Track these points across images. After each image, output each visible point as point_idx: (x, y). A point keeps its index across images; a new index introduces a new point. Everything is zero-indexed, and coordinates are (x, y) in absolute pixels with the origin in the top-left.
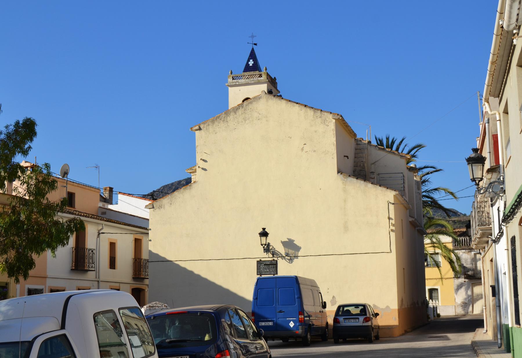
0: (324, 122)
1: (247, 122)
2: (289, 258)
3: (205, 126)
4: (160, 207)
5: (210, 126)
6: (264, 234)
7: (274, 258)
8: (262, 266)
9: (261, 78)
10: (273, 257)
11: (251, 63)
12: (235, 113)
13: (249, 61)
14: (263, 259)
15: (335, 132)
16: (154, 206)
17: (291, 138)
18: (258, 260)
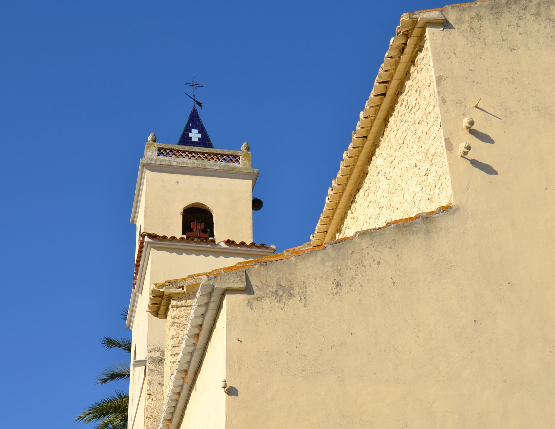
3: (466, 16)
4: (284, 292)
5: (485, 23)
9: (236, 164)
11: (195, 135)
13: (188, 130)
16: (254, 282)
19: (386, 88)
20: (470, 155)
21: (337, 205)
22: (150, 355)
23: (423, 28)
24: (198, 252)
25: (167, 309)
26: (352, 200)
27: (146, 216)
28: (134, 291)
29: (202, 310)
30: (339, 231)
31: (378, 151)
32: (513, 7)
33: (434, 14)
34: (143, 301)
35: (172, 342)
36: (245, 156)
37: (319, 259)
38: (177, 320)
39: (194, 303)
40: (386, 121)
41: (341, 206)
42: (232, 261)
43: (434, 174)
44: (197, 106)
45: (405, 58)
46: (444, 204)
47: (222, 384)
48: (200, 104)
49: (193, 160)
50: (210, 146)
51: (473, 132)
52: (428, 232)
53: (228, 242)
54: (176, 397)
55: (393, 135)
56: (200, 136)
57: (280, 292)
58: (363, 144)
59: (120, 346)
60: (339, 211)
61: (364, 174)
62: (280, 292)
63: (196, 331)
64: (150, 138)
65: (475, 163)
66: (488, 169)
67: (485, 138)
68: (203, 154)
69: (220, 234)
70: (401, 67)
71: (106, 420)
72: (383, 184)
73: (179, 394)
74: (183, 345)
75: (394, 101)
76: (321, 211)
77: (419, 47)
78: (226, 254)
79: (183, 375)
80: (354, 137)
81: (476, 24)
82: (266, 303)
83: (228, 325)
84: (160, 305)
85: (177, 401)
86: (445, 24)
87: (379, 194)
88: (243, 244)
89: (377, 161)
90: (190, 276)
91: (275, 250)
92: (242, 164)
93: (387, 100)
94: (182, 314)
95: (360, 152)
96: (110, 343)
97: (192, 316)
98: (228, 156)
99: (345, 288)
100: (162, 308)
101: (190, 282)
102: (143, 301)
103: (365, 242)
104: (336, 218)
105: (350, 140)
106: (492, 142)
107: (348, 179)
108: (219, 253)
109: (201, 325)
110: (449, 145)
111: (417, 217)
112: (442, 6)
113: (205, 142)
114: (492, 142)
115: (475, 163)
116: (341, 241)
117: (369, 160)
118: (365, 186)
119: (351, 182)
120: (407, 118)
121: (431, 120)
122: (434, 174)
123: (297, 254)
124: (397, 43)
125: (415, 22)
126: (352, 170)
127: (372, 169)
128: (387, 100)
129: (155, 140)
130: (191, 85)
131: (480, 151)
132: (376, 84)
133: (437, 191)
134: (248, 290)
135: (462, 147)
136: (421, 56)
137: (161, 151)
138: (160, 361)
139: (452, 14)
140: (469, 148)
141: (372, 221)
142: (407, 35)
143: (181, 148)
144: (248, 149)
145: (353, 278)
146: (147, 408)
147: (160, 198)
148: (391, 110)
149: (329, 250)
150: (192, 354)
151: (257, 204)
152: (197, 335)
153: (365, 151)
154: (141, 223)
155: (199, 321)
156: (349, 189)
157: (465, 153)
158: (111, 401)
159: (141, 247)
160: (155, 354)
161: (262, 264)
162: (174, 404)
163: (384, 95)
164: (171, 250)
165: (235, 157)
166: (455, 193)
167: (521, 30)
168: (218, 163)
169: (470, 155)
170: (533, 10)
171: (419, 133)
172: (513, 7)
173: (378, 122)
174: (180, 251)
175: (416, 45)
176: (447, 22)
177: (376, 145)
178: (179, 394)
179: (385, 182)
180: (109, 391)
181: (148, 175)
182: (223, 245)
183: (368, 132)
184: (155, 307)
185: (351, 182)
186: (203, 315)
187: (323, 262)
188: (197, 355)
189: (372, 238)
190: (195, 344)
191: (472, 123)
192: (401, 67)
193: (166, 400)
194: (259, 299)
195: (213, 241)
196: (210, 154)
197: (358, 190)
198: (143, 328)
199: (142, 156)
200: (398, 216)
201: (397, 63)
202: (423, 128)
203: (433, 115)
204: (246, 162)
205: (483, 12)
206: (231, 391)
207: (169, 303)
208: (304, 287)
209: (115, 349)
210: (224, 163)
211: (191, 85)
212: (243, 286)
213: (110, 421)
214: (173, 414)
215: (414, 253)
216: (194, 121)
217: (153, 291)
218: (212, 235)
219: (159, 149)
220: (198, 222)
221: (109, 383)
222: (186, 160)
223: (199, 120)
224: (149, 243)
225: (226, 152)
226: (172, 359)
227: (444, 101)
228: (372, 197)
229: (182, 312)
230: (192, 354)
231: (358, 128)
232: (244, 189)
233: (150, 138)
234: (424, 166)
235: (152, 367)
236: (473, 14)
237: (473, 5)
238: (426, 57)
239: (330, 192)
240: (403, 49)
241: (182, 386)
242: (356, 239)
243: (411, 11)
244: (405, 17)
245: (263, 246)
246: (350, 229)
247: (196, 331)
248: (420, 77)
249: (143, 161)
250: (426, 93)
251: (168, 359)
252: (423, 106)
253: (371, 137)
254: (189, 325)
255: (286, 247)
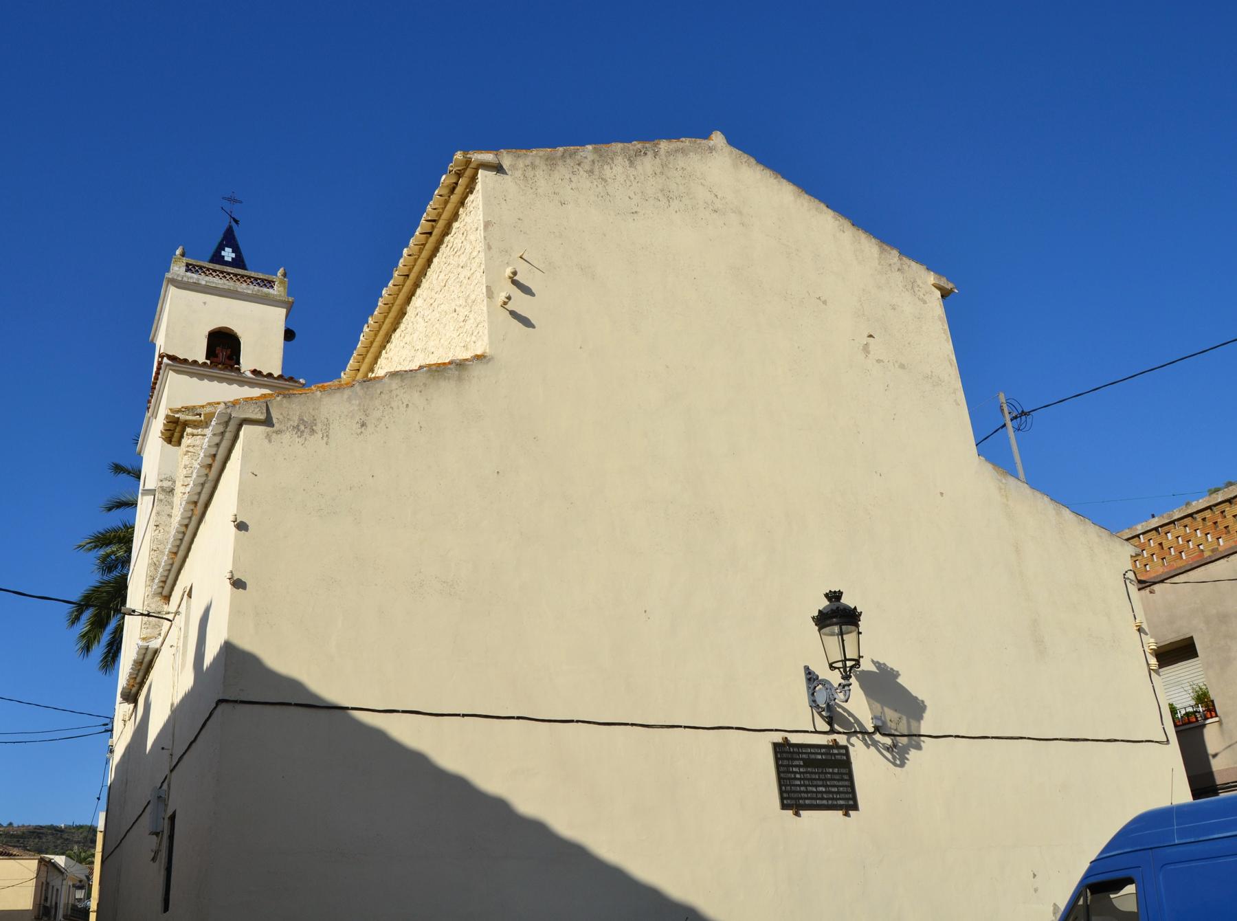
0: (912, 286)
1: (675, 204)
2: (888, 741)
3: (521, 163)
4: (305, 427)
5: (539, 173)
6: (838, 616)
7: (835, 736)
8: (797, 770)
9: (271, 291)
10: (832, 731)
11: (228, 254)
12: (632, 163)
13: (221, 247)
14: (795, 739)
15: (946, 327)
16: (275, 415)
17: (825, 302)
18: (778, 738)
19: (433, 227)
20: (510, 306)
21: (372, 343)
22: (160, 484)
23: (476, 169)
24: (221, 380)
25: (182, 437)
26: (388, 339)
27: (167, 335)
28: (148, 415)
29: (217, 439)
30: (372, 370)
31: (419, 291)
32: (568, 161)
33: (488, 157)
34: (157, 426)
35: (185, 472)
36: (281, 282)
37: (346, 396)
38: (191, 449)
39: (208, 432)
40: (429, 262)
41: (376, 344)
42: (256, 392)
43: (472, 321)
44: (233, 224)
45: (454, 198)
46: (479, 353)
47: (232, 518)
48: (236, 222)
49: (224, 281)
50: (244, 267)
51: (515, 282)
52: (460, 379)
53: (254, 372)
54: (183, 529)
55: (435, 276)
56: (233, 255)
57: (302, 427)
58: (404, 282)
59: (129, 473)
60: (373, 350)
61: (402, 314)
62: (302, 427)
63: (209, 461)
64: (178, 252)
65: (513, 314)
66: (526, 322)
67: (526, 290)
68: (236, 275)
69: (247, 362)
70: (450, 207)
71: (108, 550)
72: (421, 325)
73: (187, 526)
74: (194, 476)
75: (440, 242)
76: (355, 348)
77: (470, 189)
78: (251, 384)
79: (192, 507)
80: (396, 274)
81: (530, 173)
82: (287, 437)
83: (243, 456)
84: (175, 431)
85: (184, 533)
86: (499, 169)
87: (415, 336)
88: (270, 375)
89: (417, 302)
90: (209, 404)
91: (304, 385)
92: (277, 291)
93: (433, 239)
94: (198, 443)
95: (400, 290)
96: (118, 469)
97: (205, 446)
98: (263, 280)
99: (370, 428)
100: (176, 435)
101: (208, 410)
102: (157, 426)
103: (395, 384)
104: (370, 356)
105: (391, 277)
106: (533, 295)
107: (385, 317)
108: (243, 382)
109: (215, 456)
110: (490, 294)
111: (450, 363)
112: (497, 149)
113: (238, 262)
114: (533, 295)
115: (513, 314)
116: (371, 379)
117: (408, 300)
118: (402, 326)
119: (388, 321)
120: (451, 260)
121: (474, 266)
122: (472, 321)
123: (323, 389)
124: (448, 182)
125: (468, 162)
126: (390, 309)
127: (410, 309)
128: (433, 239)
129: (183, 255)
130: (229, 199)
131: (521, 303)
132: (423, 221)
133: (474, 338)
134: (268, 422)
135: (502, 297)
136: (471, 197)
137: (189, 267)
138: (171, 491)
139: (506, 160)
140: (509, 298)
141: (406, 363)
142: (459, 175)
143: (211, 266)
144: (285, 275)
145: (379, 420)
146: (153, 540)
147: (184, 317)
148: (436, 250)
149: (357, 387)
150: (203, 485)
151: (289, 335)
152: (210, 466)
153: (406, 289)
154: (162, 342)
155: (213, 451)
156: (385, 327)
157: (505, 303)
158: (115, 531)
159: (159, 369)
160: (166, 484)
161: (285, 396)
162: (180, 536)
163: (430, 234)
164: (192, 375)
165: (270, 282)
166: (491, 343)
167: (573, 185)
168: (251, 286)
169: (510, 306)
170: (587, 167)
171: (462, 277)
172: (568, 161)
173: (421, 262)
174: (201, 377)
175: (467, 187)
176: (501, 166)
177: (417, 285)
178: (187, 526)
179: (423, 324)
180: (114, 520)
181: (172, 290)
182: (249, 374)
183: (410, 270)
184: (168, 434)
185: (388, 321)
186: (218, 445)
187: (349, 399)
188: (208, 487)
189: (402, 380)
190: (207, 475)
191: (515, 273)
192: (450, 207)
193: (173, 532)
194: (279, 432)
195: (239, 369)
196: (242, 276)
197: (395, 330)
198: (155, 455)
199: (168, 271)
200: (433, 360)
201: (446, 202)
202: (466, 273)
203: (477, 260)
204: (281, 289)
205: (537, 161)
206: (241, 526)
207: (184, 430)
208: (327, 424)
209: (123, 476)
210: (257, 288)
211: (229, 199)
212: (262, 417)
213: (113, 552)
214: (179, 547)
215: (444, 397)
216: (229, 239)
217: (167, 417)
218: (238, 363)
219: (187, 265)
220: (223, 347)
221: (115, 512)
222: (216, 280)
223: (234, 238)
224: (167, 365)
225: (261, 276)
226: (183, 489)
227: (489, 248)
228: (408, 339)
229: (197, 441)
230: (203, 485)
231: (400, 265)
232: (276, 318)
233: (178, 252)
234: (463, 312)
235: (162, 497)
236: (528, 162)
237: (528, 153)
238: (476, 200)
239: (366, 329)
240: (454, 189)
241: (190, 518)
242: (386, 380)
243: (466, 150)
244: (459, 156)
245: (291, 379)
246: (382, 369)
247: (209, 461)
248: (468, 219)
249: (168, 275)
250: (472, 237)
251: (179, 489)
252: (468, 250)
253: (413, 276)
254: (202, 455)
255: (315, 382)
